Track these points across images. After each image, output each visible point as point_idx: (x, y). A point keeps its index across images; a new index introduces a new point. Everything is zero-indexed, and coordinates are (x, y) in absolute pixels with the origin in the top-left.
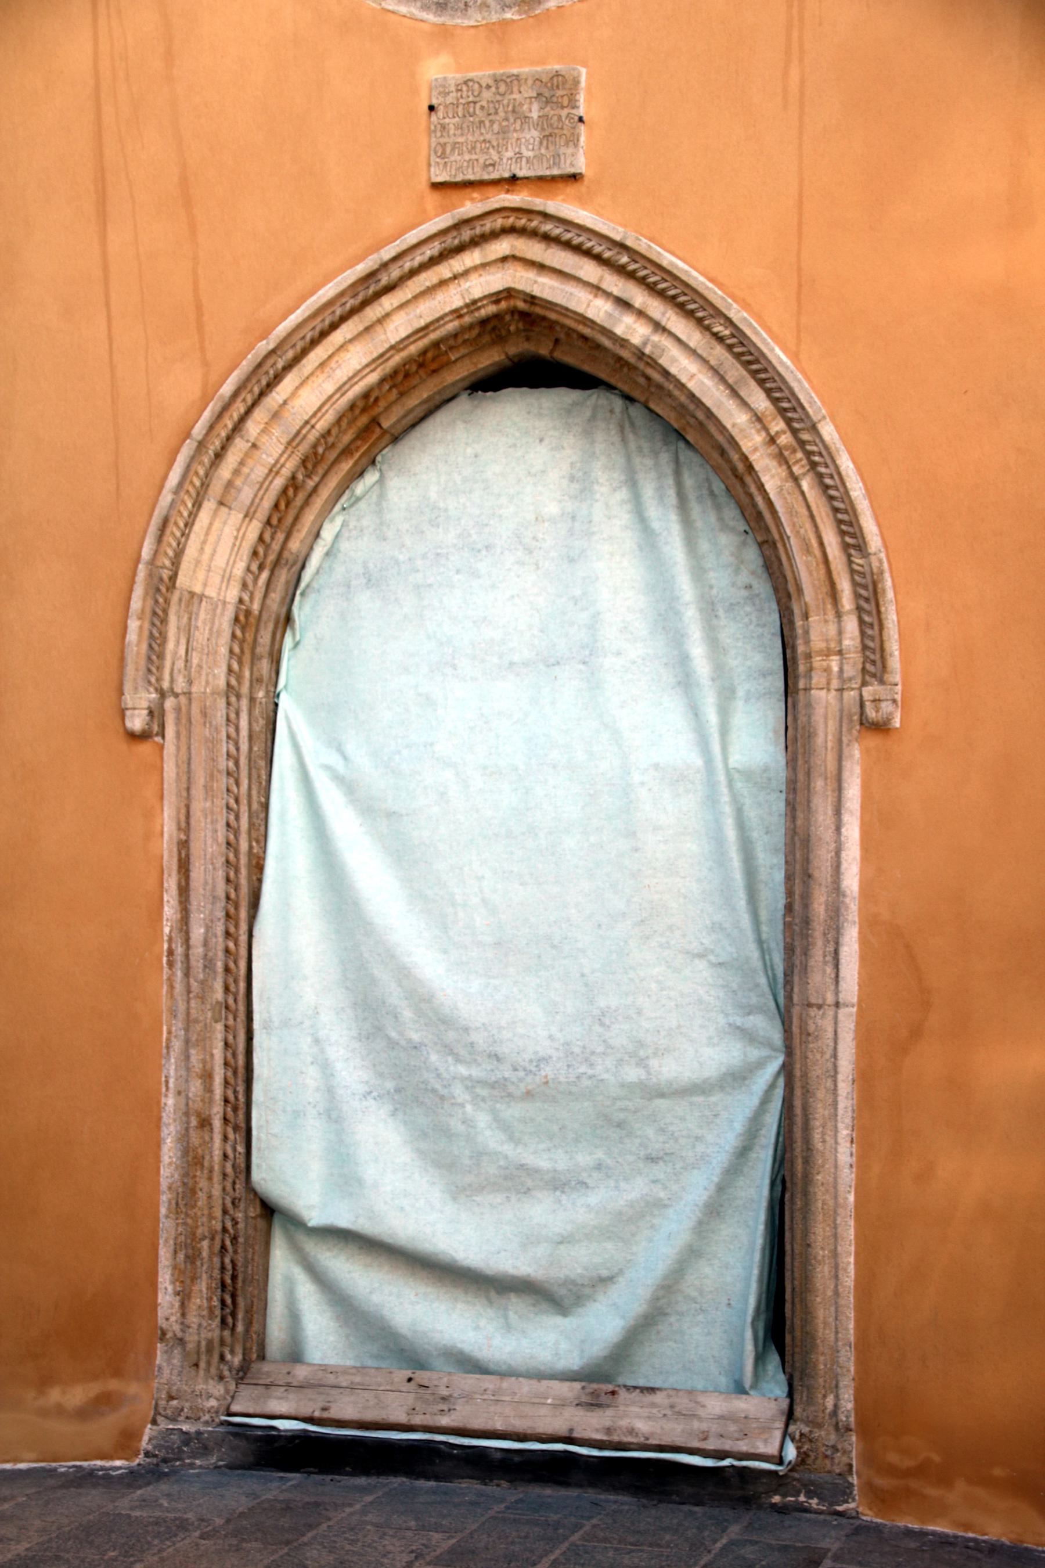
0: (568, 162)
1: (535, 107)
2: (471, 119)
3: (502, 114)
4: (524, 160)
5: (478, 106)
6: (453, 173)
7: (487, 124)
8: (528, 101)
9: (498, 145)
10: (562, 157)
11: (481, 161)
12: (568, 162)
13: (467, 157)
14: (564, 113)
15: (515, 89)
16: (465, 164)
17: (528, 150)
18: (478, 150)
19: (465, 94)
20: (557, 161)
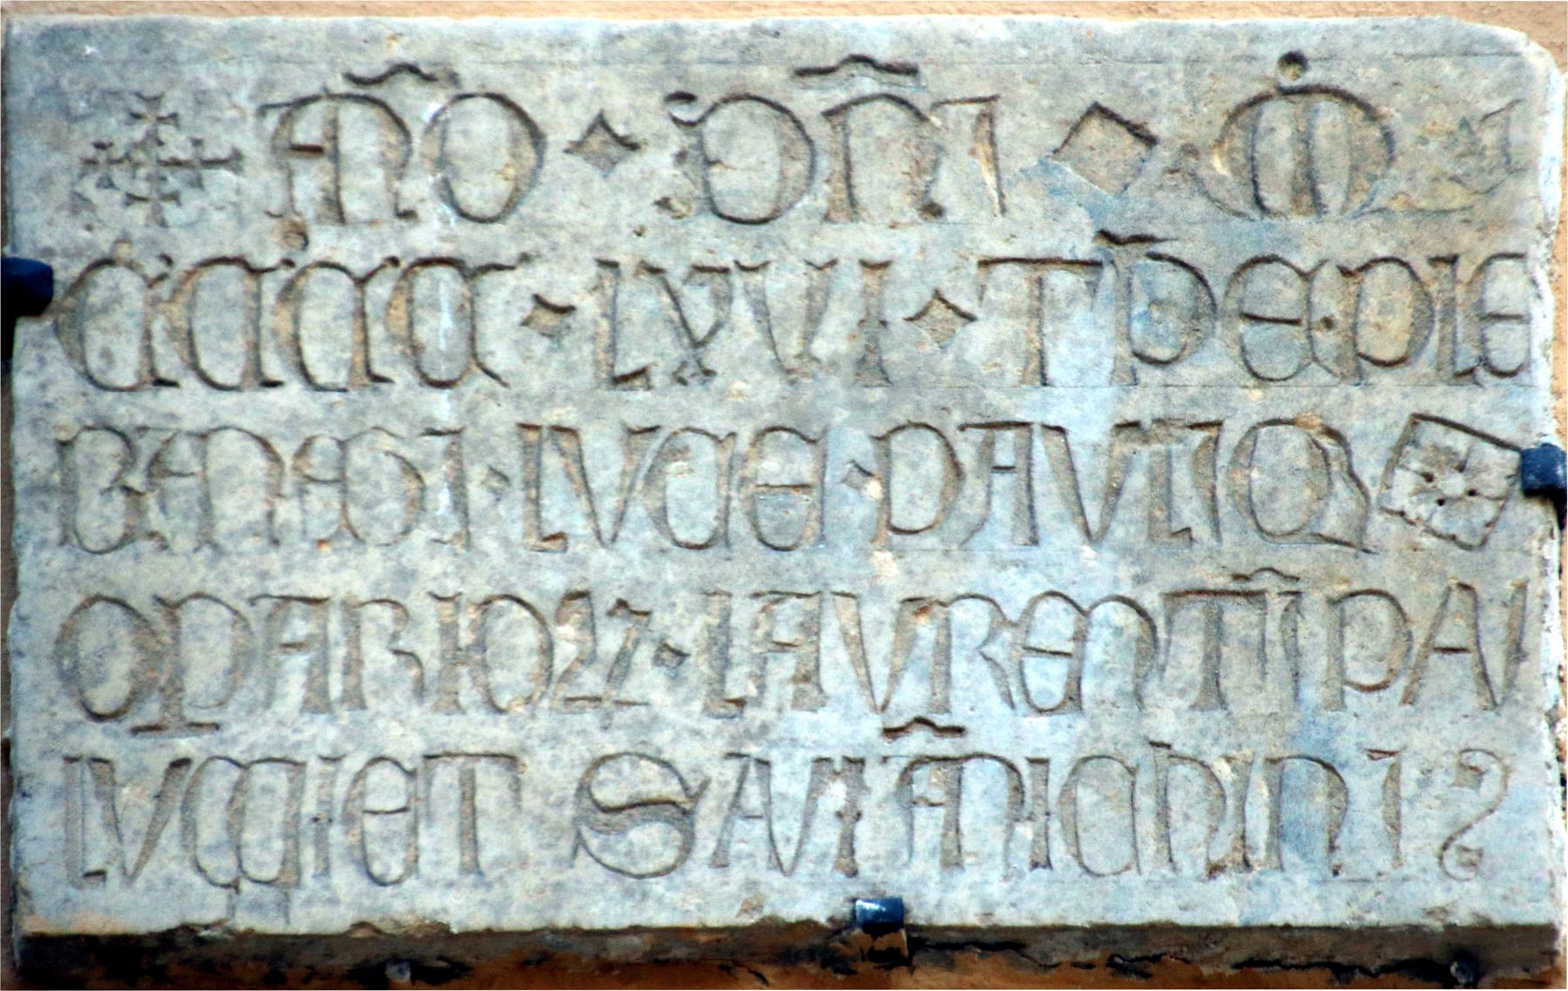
0: (1424, 825)
1: (1084, 341)
2: (442, 407)
3: (747, 385)
4: (981, 782)
5: (503, 300)
6: (265, 860)
7: (606, 458)
8: (1012, 284)
9: (720, 644)
10: (1364, 785)
11: (553, 770)
12: (1424, 825)
13: (404, 729)
14: (1374, 411)
15: (882, 181)
16: (387, 789)
17: (1018, 696)
18: (512, 678)
19: (364, 191)
20: (1314, 808)
